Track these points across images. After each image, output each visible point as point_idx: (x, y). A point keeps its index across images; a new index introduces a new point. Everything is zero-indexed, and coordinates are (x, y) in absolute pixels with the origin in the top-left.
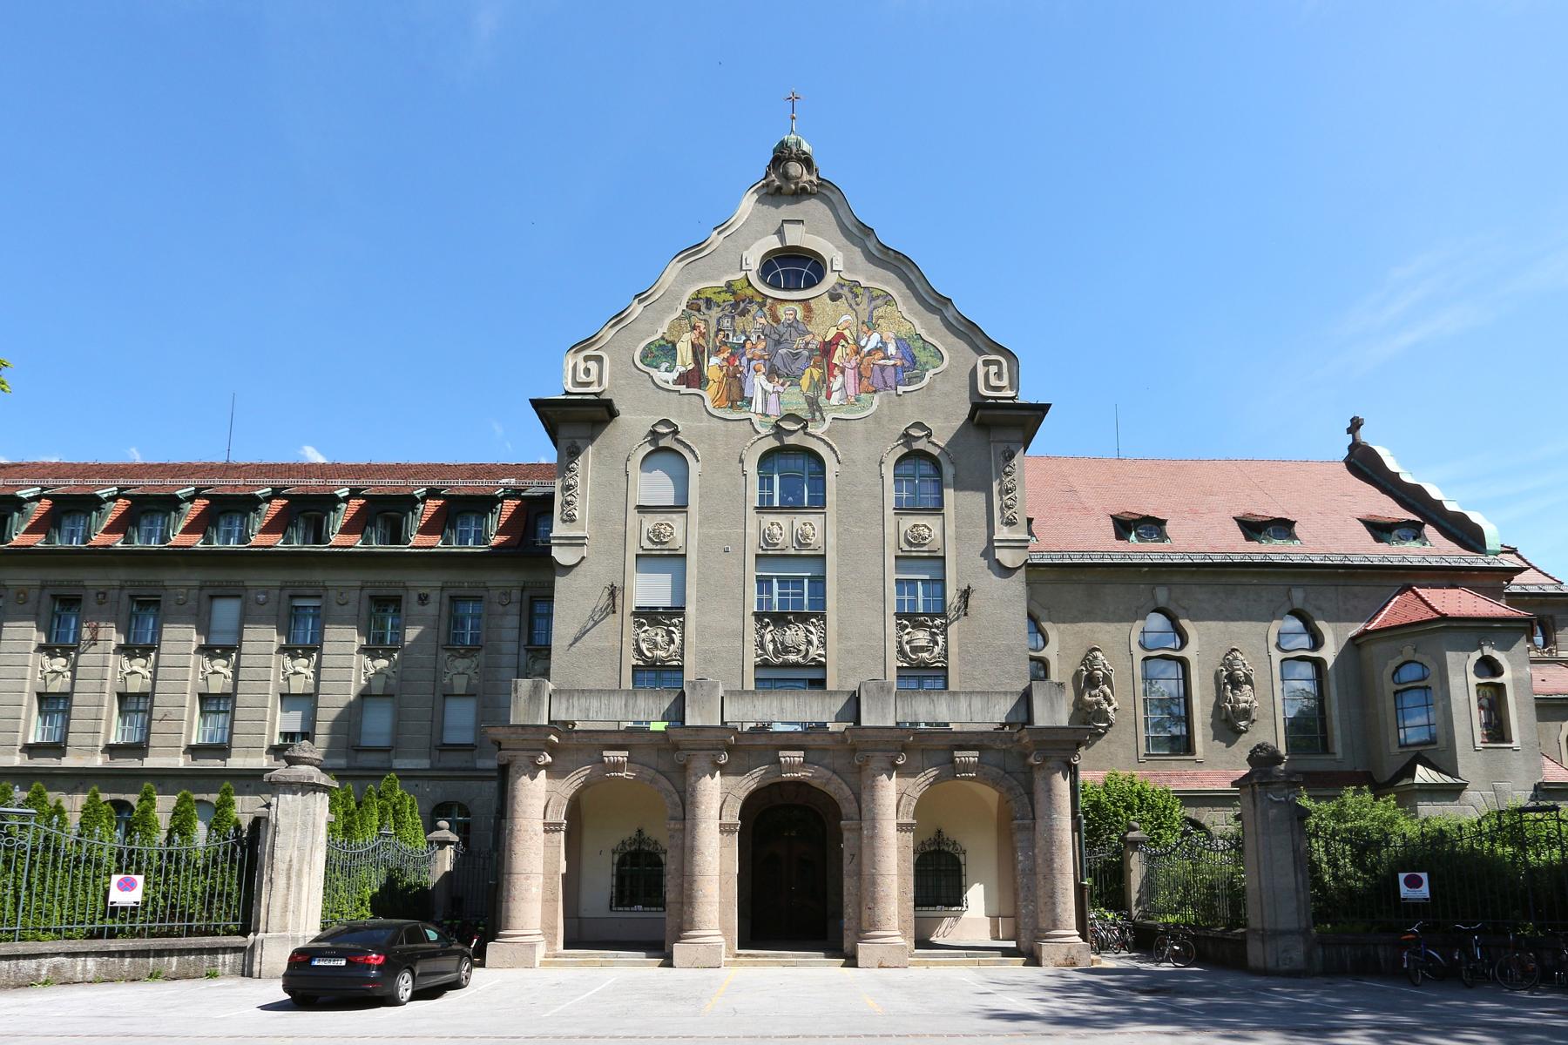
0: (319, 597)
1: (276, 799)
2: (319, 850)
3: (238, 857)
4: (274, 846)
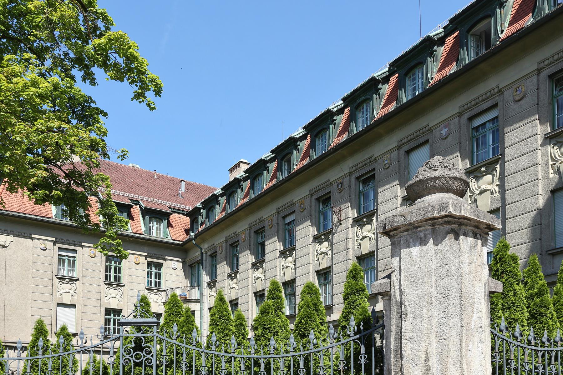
0: (495, 106)
1: (397, 259)
2: (476, 340)
3: (363, 361)
4: (401, 338)
